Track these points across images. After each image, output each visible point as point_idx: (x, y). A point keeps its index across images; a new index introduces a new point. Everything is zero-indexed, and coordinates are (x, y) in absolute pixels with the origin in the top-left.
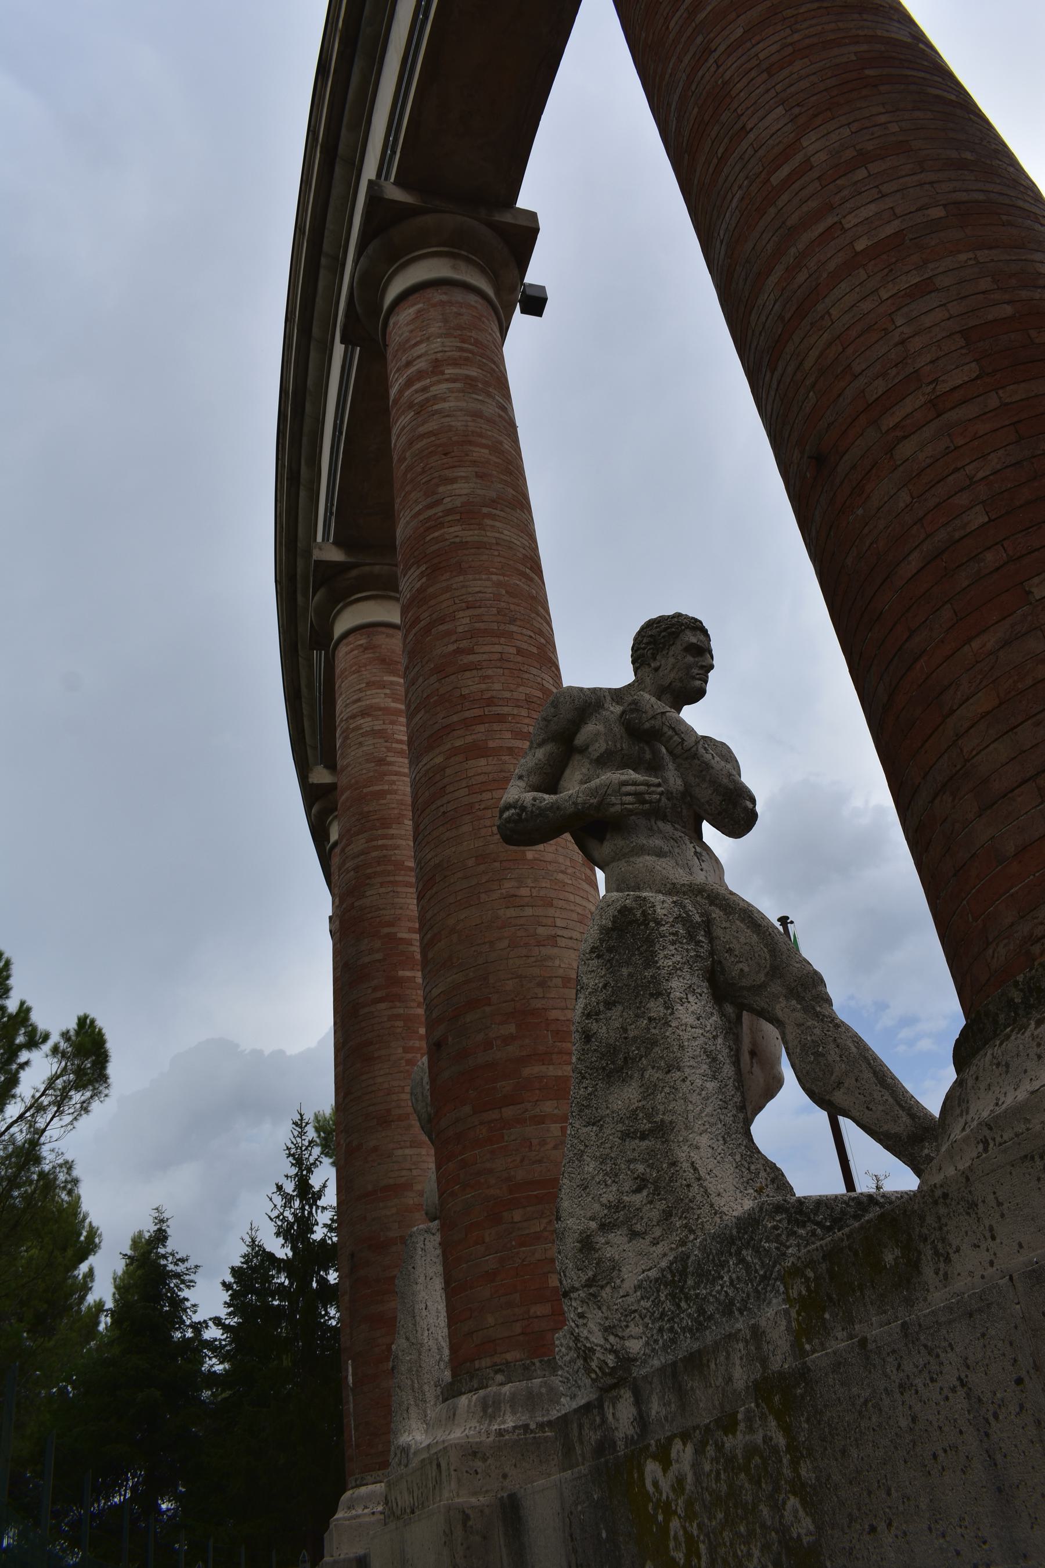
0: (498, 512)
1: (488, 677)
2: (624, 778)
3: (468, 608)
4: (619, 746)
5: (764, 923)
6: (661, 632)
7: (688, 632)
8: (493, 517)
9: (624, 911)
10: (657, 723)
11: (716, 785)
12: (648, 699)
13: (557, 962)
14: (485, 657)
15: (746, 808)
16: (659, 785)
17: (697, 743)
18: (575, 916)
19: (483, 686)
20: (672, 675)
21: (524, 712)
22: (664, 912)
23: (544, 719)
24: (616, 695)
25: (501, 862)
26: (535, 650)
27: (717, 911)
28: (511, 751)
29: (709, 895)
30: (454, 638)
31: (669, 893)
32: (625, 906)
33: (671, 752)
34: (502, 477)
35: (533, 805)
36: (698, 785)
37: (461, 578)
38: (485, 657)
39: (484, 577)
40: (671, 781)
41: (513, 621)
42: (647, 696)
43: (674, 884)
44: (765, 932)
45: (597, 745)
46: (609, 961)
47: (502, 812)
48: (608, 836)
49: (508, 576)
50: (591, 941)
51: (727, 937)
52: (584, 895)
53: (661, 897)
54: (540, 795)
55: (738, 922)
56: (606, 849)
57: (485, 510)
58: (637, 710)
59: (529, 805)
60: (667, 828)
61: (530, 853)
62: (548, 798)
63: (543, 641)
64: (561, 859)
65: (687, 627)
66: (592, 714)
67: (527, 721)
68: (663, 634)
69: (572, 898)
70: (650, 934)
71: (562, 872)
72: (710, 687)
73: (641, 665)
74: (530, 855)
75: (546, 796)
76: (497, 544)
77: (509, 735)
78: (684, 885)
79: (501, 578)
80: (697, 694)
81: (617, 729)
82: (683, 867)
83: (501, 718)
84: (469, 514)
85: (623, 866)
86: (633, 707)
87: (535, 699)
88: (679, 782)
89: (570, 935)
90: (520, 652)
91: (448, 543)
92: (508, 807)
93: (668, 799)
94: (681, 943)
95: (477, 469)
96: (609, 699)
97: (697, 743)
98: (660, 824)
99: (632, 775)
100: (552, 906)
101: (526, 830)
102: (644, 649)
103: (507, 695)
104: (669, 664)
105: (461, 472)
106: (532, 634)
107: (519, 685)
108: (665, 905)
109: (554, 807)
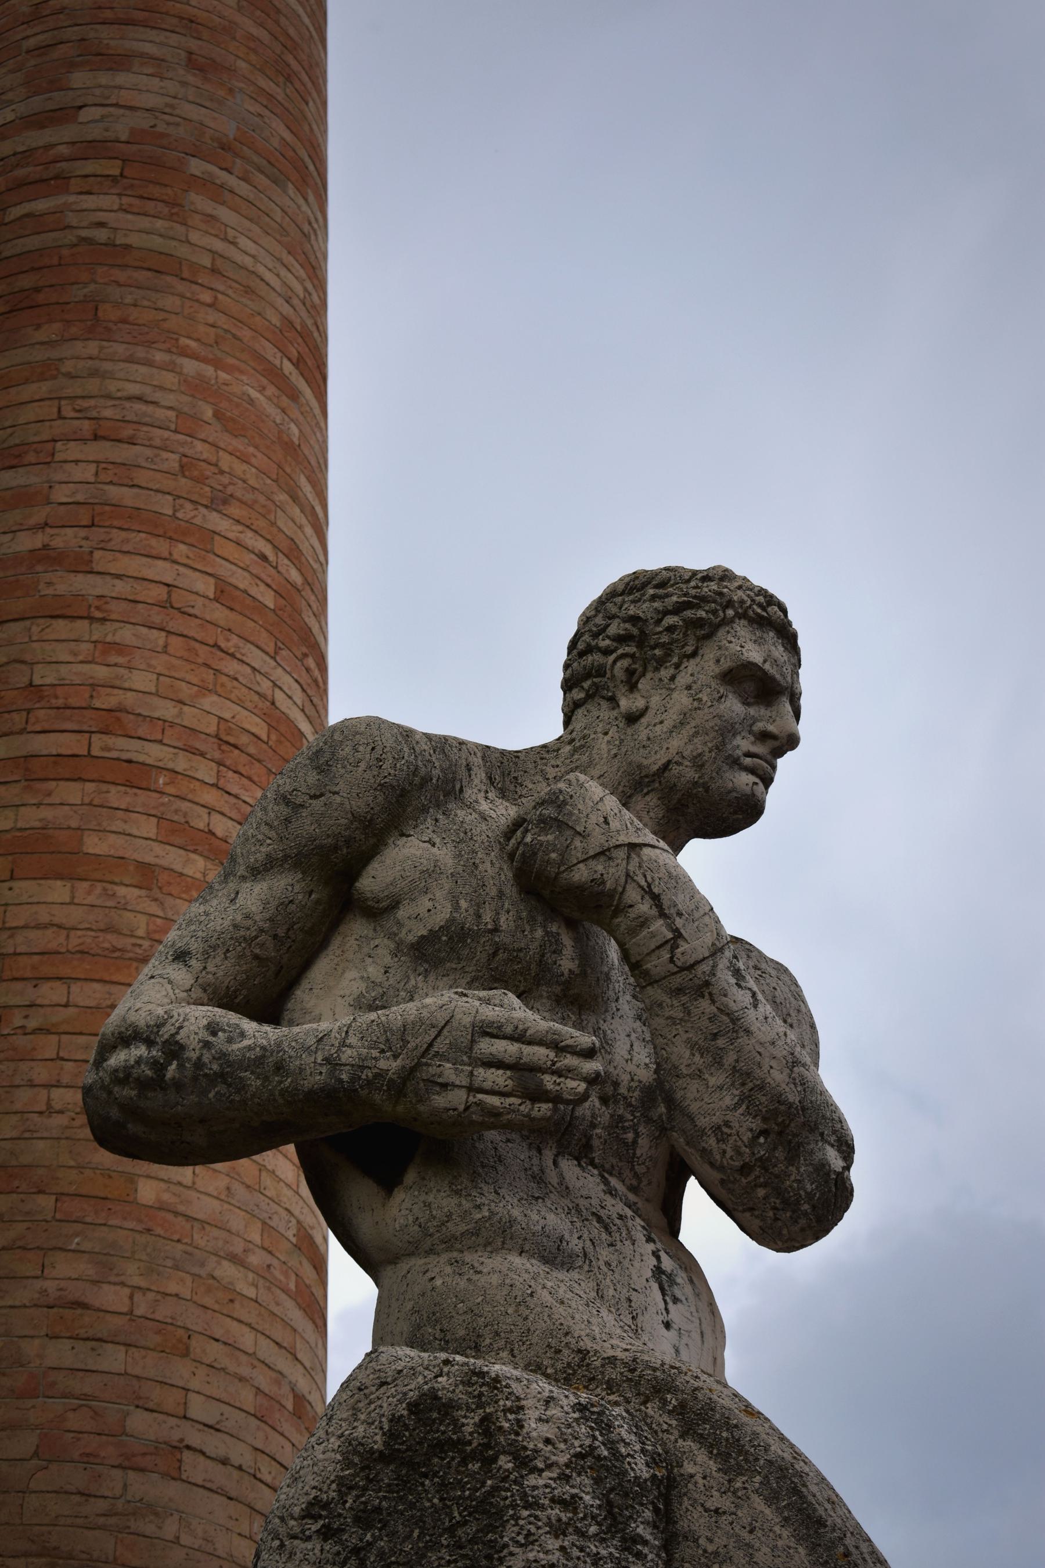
0: (232, 181)
1: (120, 648)
2: (489, 1013)
3: (96, 438)
4: (487, 917)
5: (833, 1518)
6: (666, 613)
7: (742, 629)
8: (217, 192)
9: (428, 1407)
10: (612, 873)
11: (748, 1083)
12: (596, 798)
13: (170, 1528)
14: (121, 588)
15: (822, 1168)
16: (589, 1053)
17: (716, 951)
18: (247, 1398)
19: (101, 672)
20: (676, 743)
21: (206, 771)
22: (547, 1431)
23: (285, 799)
24: (505, 769)
25: (60, 1196)
26: (269, 599)
27: (702, 1456)
28: (147, 875)
29: (683, 1405)
30: (40, 514)
31: (566, 1378)
32: (433, 1394)
33: (634, 965)
34: (263, 82)
35: (207, 1045)
36: (698, 1075)
37: (92, 347)
38: (121, 588)
39: (159, 357)
40: (621, 1049)
41: (220, 502)
42: (596, 789)
43: (583, 1353)
44: (832, 1545)
45: (425, 903)
46: (356, 1551)
47: (106, 1049)
48: (411, 1176)
49: (229, 369)
50: (311, 1481)
51: (720, 1541)
52: (286, 1339)
53: (543, 1386)
54: (233, 1018)
55: (758, 1502)
56: (401, 1211)
57: (196, 166)
58: (561, 825)
59: (193, 1042)
60: (586, 1182)
61: (154, 1183)
62: (256, 1033)
63: (295, 576)
64: (236, 1221)
65: (744, 616)
66: (425, 810)
67: (210, 797)
68: (670, 620)
69: (247, 1339)
70: (495, 1489)
71: (235, 1259)
72: (774, 798)
73: (589, 697)
74: (147, 1192)
75: (249, 1026)
76: (214, 271)
77: (148, 828)
78: (612, 1360)
79: (209, 371)
80: (735, 814)
81: (495, 871)
82: (615, 1308)
83: (135, 776)
84: (149, 167)
85: (439, 1272)
86: (550, 811)
87: (244, 739)
88: (643, 1055)
89: (221, 1452)
90: (224, 593)
91: (70, 237)
92: (127, 1038)
93: (604, 1100)
94: (582, 1534)
95: (193, 44)
96: (479, 775)
97: (716, 951)
98: (569, 1168)
99: (510, 1008)
100: (186, 1353)
101: (168, 1113)
102: (607, 652)
103: (167, 710)
104: (676, 710)
105: (145, 42)
106: (268, 551)
107: (205, 689)
108: (554, 1411)
109: (269, 1063)
